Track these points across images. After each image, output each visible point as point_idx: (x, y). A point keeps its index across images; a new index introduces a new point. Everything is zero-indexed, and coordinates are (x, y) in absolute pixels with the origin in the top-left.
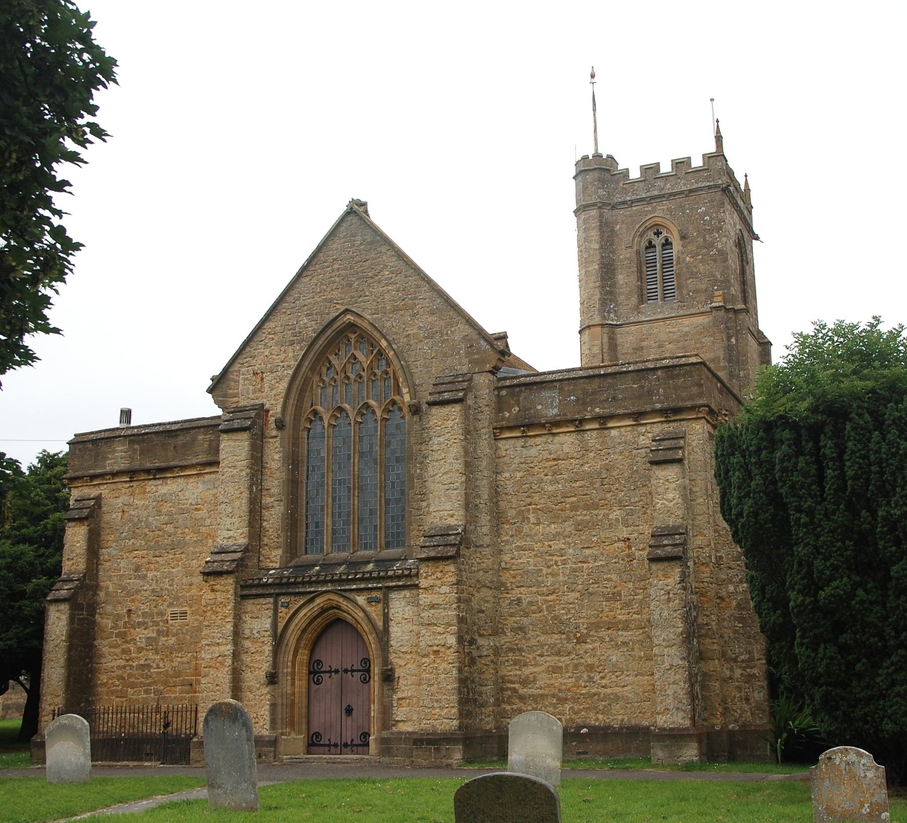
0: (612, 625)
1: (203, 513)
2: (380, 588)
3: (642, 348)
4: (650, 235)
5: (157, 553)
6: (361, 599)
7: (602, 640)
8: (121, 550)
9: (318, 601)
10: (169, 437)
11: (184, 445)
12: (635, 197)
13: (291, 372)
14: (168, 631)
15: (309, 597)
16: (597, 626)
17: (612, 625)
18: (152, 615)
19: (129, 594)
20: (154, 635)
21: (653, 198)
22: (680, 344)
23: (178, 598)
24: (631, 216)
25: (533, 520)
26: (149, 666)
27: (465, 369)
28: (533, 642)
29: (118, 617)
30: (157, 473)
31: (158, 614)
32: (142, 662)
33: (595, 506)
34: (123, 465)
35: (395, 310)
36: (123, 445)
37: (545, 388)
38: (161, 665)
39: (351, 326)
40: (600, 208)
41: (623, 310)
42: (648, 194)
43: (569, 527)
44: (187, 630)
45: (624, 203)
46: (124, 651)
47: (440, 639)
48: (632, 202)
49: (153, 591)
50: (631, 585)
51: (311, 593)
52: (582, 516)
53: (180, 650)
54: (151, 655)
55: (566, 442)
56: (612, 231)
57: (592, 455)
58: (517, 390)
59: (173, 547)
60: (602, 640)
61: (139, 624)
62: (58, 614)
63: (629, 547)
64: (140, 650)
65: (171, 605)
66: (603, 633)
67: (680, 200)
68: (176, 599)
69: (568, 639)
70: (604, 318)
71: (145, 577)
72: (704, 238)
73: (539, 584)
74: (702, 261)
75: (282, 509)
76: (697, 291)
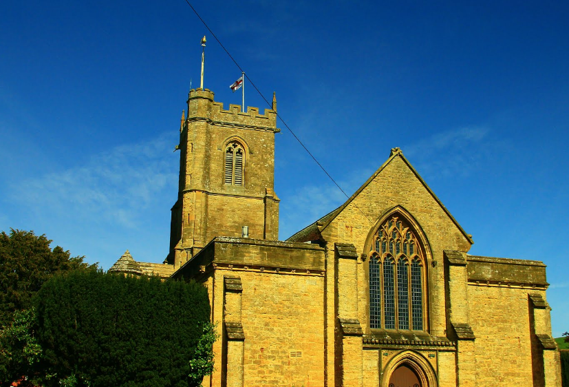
0: (513, 375)
1: (310, 298)
2: (435, 350)
3: (223, 210)
4: (231, 145)
5: (280, 317)
6: (425, 354)
7: (509, 380)
8: (256, 312)
9: (403, 353)
10: (287, 251)
11: (297, 257)
12: (226, 121)
13: (368, 231)
14: (289, 363)
15: (400, 351)
16: (507, 374)
17: (513, 375)
18: (278, 352)
19: (261, 339)
20: (280, 364)
21: (236, 125)
22: (244, 213)
23: (294, 344)
24: (222, 131)
25: (481, 324)
26: (277, 382)
27: (456, 249)
28: (482, 380)
29: (255, 352)
30: (283, 270)
31: (282, 352)
32: (273, 379)
33: (505, 321)
34: (257, 261)
35: (421, 211)
36: (256, 249)
37: (485, 265)
38: (286, 381)
39: (396, 214)
40: (207, 122)
41: (212, 185)
42: (234, 122)
43: (495, 329)
44: (302, 363)
45: (219, 123)
46: (260, 372)
47: (468, 377)
48: (225, 124)
49: (278, 338)
50: (520, 358)
51: (400, 349)
52: (501, 325)
53: (298, 373)
54: (278, 375)
55: (493, 291)
56: (211, 137)
57: (503, 298)
58: (474, 263)
59: (290, 314)
60: (509, 380)
61: (269, 357)
62: (235, 347)
63: (519, 341)
64: (271, 372)
65: (291, 347)
66: (510, 377)
67: (252, 131)
68: (293, 345)
69: (496, 379)
70: (204, 186)
71: (272, 330)
72: (262, 156)
73: (484, 354)
74: (260, 168)
75: (365, 303)
76: (255, 185)
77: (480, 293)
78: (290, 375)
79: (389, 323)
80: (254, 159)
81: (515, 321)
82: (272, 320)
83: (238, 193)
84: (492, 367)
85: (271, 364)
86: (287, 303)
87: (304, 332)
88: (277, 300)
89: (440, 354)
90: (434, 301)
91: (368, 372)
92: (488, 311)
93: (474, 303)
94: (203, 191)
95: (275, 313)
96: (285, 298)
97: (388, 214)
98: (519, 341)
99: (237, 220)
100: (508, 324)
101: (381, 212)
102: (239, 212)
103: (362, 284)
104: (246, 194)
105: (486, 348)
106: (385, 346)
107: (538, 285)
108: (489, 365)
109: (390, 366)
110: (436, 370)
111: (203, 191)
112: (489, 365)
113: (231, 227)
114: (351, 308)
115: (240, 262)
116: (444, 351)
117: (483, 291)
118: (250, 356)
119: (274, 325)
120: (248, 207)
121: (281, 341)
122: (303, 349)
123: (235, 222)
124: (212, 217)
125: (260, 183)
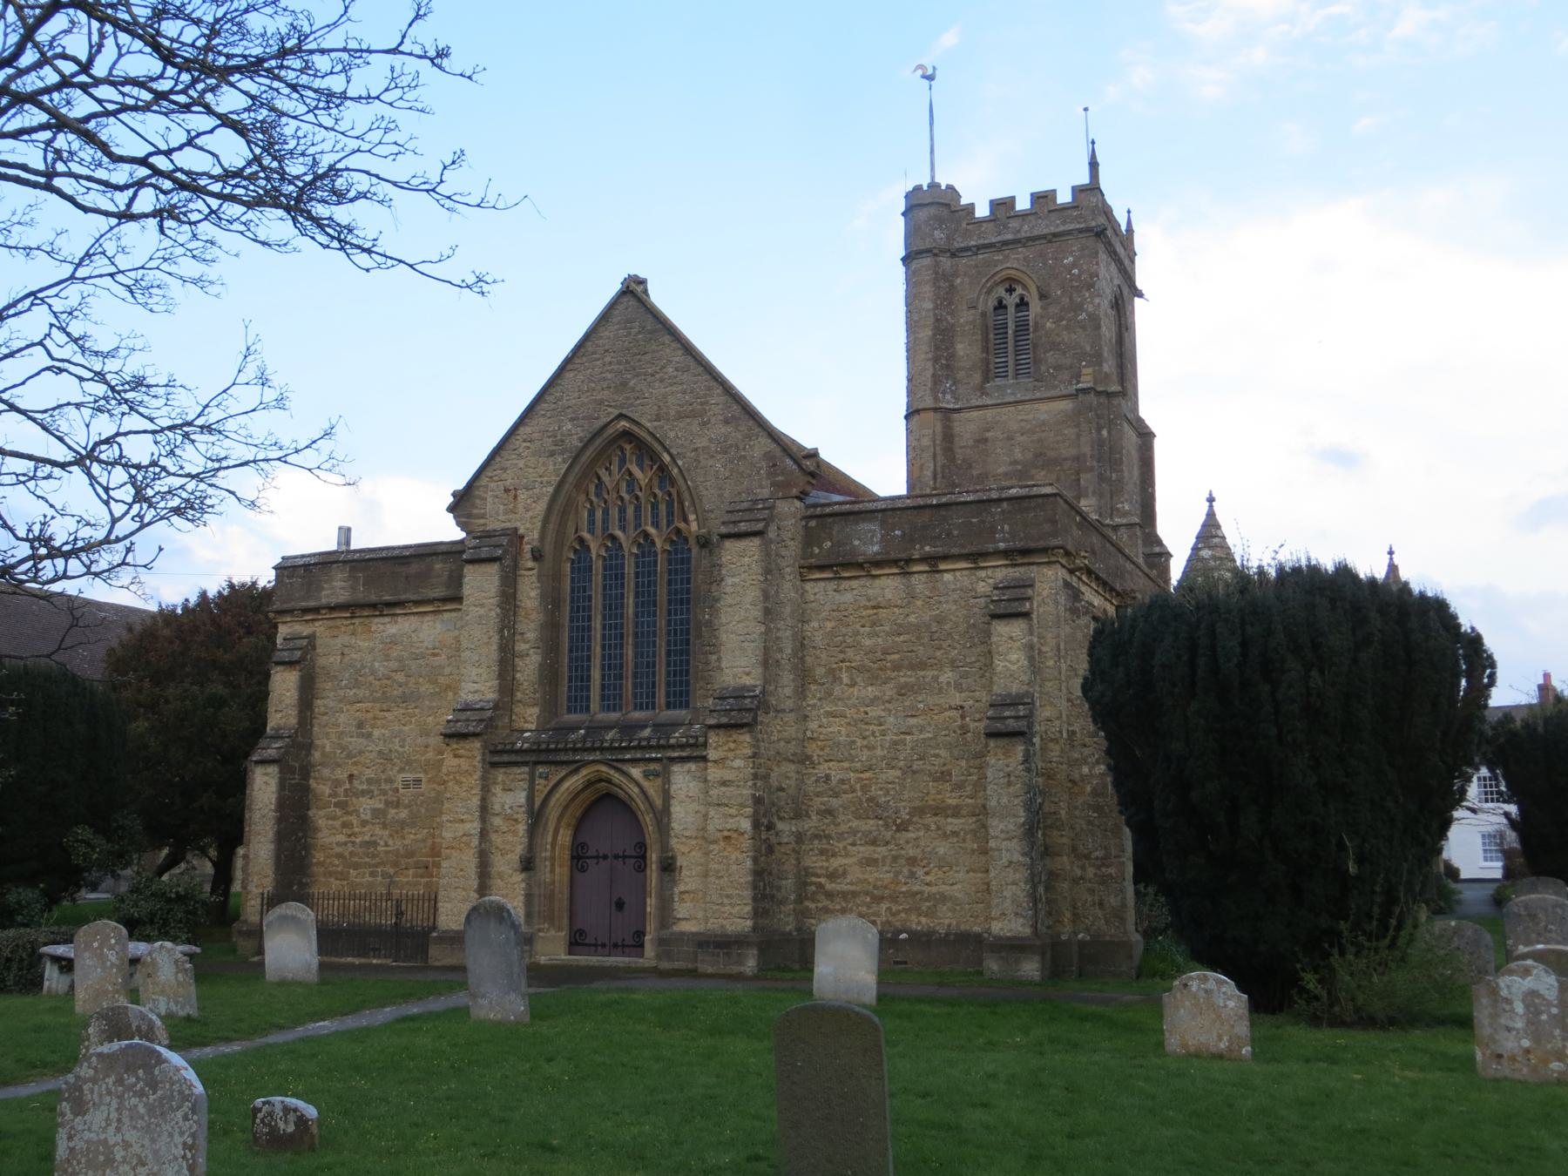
0: (939, 811)
2: (656, 760)
4: (1001, 291)
5: (385, 706)
6: (636, 772)
7: (927, 827)
8: (341, 701)
9: (584, 772)
12: (981, 242)
13: (551, 489)
18: (378, 781)
19: (349, 756)
20: (381, 806)
21: (1005, 243)
22: (1035, 437)
23: (409, 762)
25: (846, 680)
26: (375, 844)
27: (765, 493)
28: (843, 828)
32: (367, 838)
33: (922, 666)
34: (343, 597)
37: (864, 520)
39: (626, 435)
43: (889, 691)
46: (345, 825)
48: (979, 248)
49: (380, 752)
50: (963, 763)
52: (907, 677)
53: (413, 825)
54: (378, 831)
55: (888, 586)
56: (952, 286)
57: (919, 603)
59: (405, 699)
60: (927, 827)
61: (363, 793)
63: (963, 717)
64: (364, 823)
65: (402, 770)
66: (929, 820)
68: (409, 763)
69: (886, 826)
70: (936, 399)
71: (369, 736)
73: (851, 759)
74: (1067, 328)
76: (1058, 368)
77: (848, 597)
78: (399, 828)
79: (611, 700)
80: (1054, 310)
81: (953, 662)
82: (370, 715)
83: (1019, 397)
84: (874, 791)
85: (366, 805)
86: (400, 677)
87: (427, 735)
88: (382, 671)
89: (676, 768)
90: (700, 636)
91: (508, 818)
92: (868, 642)
93: (829, 625)
94: (935, 410)
95: (375, 701)
96: (394, 665)
97: (649, 438)
98: (963, 717)
99: (1019, 456)
100: (930, 673)
101: (581, 439)
102: (1022, 439)
103: (534, 616)
104: (1038, 395)
105: (859, 743)
106: (543, 757)
107: (1025, 552)
108: (865, 789)
109: (553, 801)
110: (658, 802)
111: (935, 410)
112: (865, 789)
113: (1007, 475)
114: (484, 676)
115: (312, 604)
116: (683, 760)
117: (853, 592)
118: (328, 791)
119: (373, 727)
120: (1044, 423)
121: (385, 756)
122: (426, 772)
123: (1015, 462)
124: (964, 460)
125: (1068, 362)
